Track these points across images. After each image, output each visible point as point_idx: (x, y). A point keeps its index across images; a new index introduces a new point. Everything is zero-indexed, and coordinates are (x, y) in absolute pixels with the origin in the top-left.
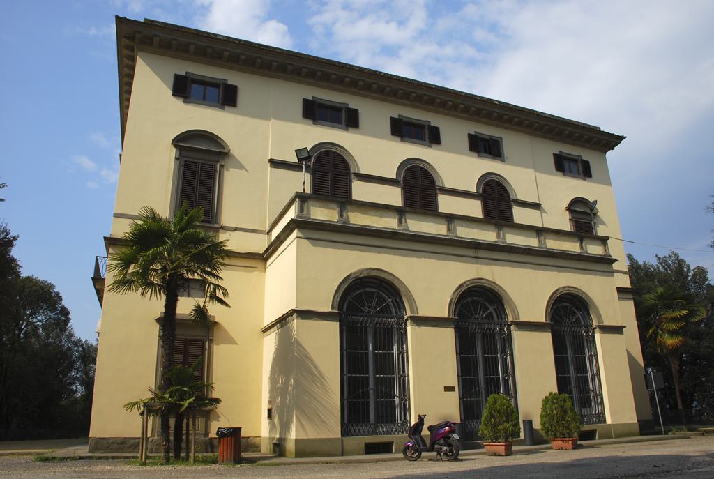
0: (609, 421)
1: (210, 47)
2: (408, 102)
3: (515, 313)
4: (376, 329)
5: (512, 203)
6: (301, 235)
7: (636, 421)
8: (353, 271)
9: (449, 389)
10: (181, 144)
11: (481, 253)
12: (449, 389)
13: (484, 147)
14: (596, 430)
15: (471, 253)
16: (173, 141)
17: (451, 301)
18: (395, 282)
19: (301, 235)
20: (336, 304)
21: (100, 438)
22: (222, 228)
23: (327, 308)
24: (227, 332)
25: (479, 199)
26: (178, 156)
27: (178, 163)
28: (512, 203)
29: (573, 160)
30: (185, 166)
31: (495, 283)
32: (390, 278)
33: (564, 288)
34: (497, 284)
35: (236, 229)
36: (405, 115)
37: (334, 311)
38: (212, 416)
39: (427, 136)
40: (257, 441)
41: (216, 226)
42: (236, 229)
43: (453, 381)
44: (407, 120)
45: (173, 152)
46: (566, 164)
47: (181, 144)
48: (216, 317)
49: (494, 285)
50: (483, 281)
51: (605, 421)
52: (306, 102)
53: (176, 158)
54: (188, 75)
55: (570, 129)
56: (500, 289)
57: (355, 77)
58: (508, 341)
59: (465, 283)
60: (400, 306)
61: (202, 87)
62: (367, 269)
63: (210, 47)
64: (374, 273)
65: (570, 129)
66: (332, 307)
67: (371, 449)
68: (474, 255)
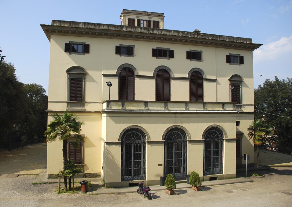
0: (224, 173)
1: (77, 31)
2: (161, 41)
3: (189, 137)
4: (135, 146)
5: (204, 80)
6: (107, 116)
7: (235, 173)
8: (126, 127)
9: (160, 165)
10: (68, 72)
11: (177, 115)
12: (160, 165)
13: (193, 56)
14: (217, 177)
15: (173, 115)
16: (66, 72)
17: (163, 135)
18: (142, 130)
19: (107, 116)
20: (120, 139)
21: (51, 175)
22: (86, 102)
23: (117, 141)
24: (90, 140)
25: (188, 80)
26: (68, 77)
27: (68, 80)
28: (204, 80)
29: (235, 56)
30: (71, 80)
31: (182, 126)
32: (140, 128)
33: (212, 125)
34: (183, 127)
35: (91, 103)
36: (158, 47)
37: (119, 142)
38: (85, 167)
39: (168, 55)
40: (100, 174)
41: (84, 102)
42: (91, 103)
43: (162, 162)
44: (159, 49)
45: (66, 76)
46: (232, 58)
47: (68, 72)
48: (85, 135)
49: (182, 127)
50: (177, 126)
51: (222, 173)
52: (117, 47)
53: (68, 78)
54: (70, 42)
55: (234, 44)
56: (184, 129)
57: (137, 35)
58: (186, 146)
59: (170, 127)
60: (144, 137)
61: (76, 45)
62: (132, 126)
63: (77, 31)
64: (134, 127)
65: (234, 44)
66: (119, 140)
67: (212, 179)
68: (174, 116)
